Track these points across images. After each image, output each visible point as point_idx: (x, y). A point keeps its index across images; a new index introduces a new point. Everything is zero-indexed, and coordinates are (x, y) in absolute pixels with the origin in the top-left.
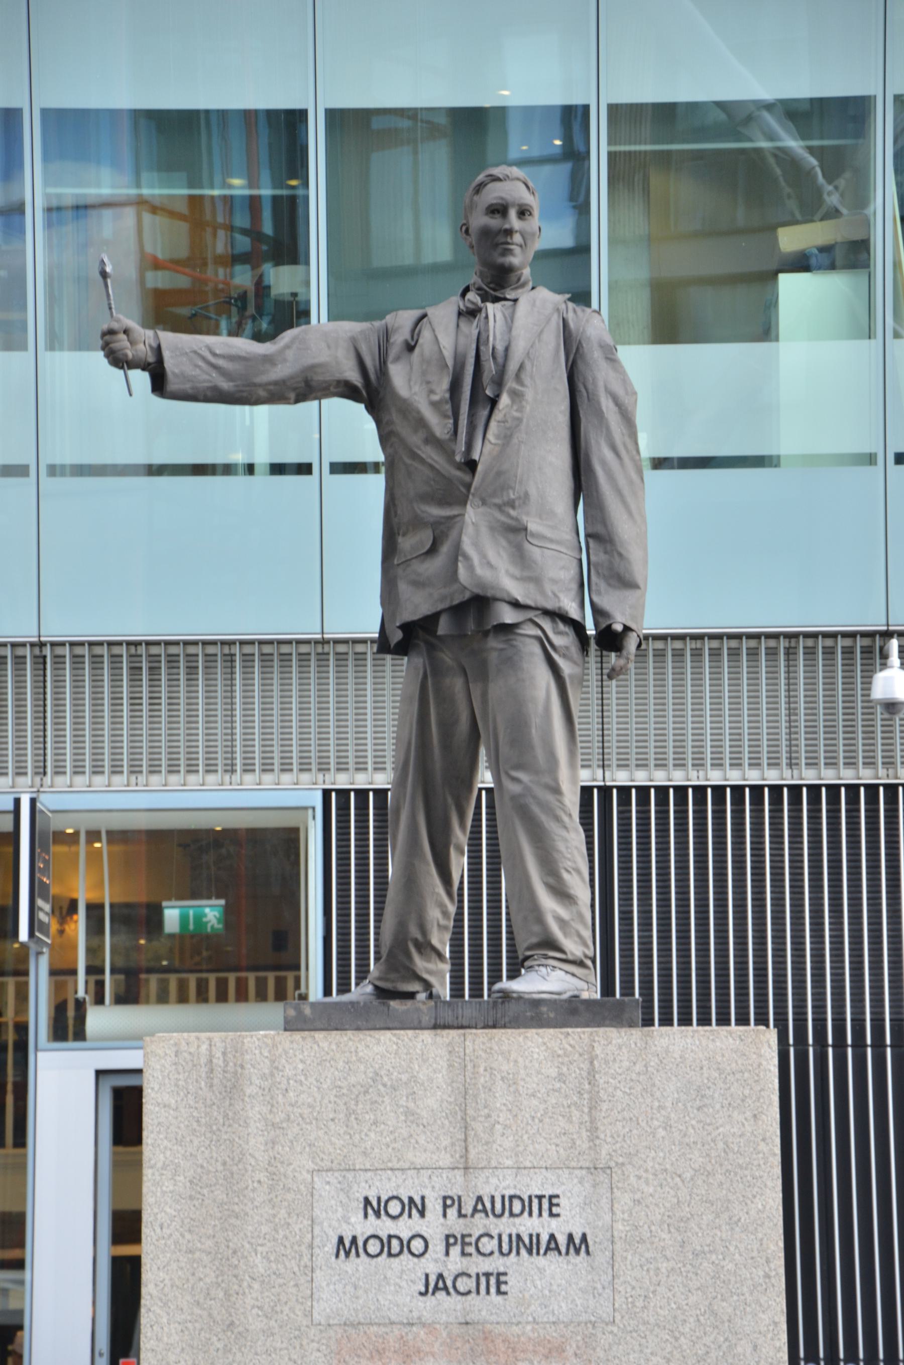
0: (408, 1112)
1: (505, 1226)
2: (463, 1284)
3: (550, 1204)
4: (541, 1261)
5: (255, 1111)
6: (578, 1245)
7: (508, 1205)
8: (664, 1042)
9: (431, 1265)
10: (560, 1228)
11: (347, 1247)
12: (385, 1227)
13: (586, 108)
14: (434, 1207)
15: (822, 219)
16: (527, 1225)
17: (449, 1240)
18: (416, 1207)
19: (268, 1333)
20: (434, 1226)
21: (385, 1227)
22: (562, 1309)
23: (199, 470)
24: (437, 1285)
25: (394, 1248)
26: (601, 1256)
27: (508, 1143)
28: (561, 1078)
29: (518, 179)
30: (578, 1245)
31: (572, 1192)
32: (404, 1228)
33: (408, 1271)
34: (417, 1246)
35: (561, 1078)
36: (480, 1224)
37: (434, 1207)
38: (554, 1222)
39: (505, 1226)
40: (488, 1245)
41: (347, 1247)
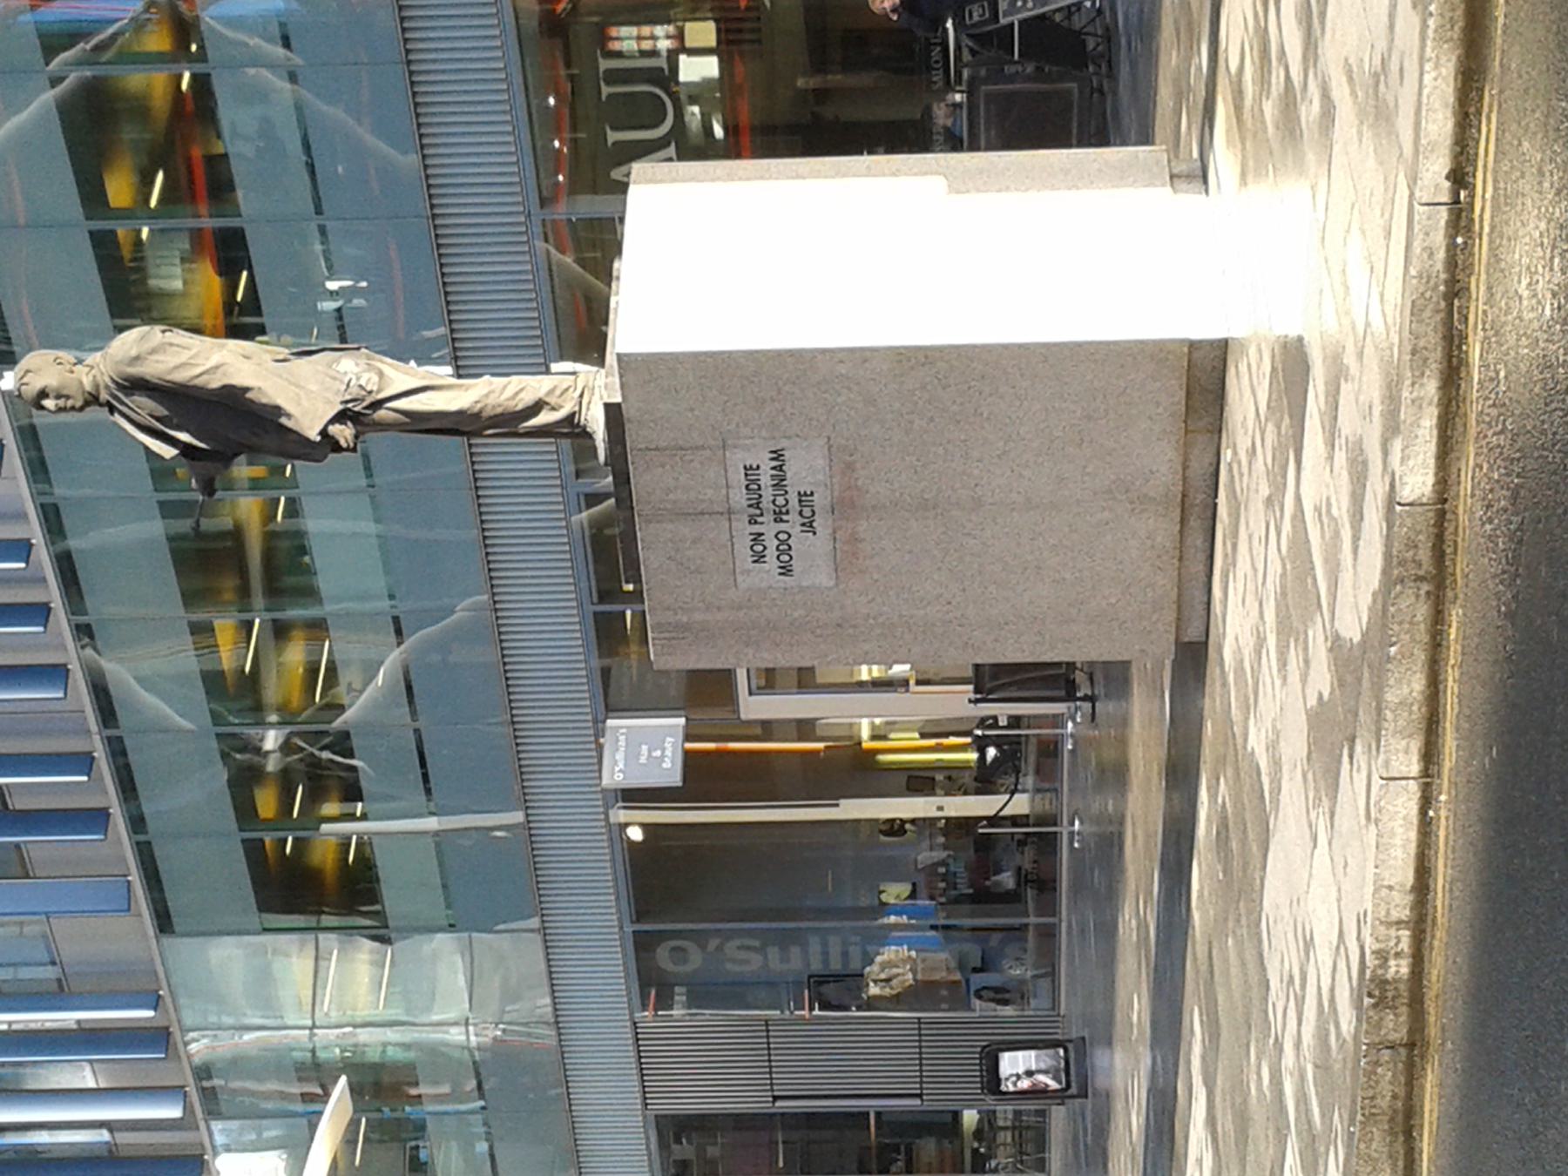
0: (694, 542)
1: (768, 494)
4: (789, 475)
5: (698, 616)
6: (777, 455)
7: (752, 486)
8: (632, 412)
9: (796, 530)
10: (767, 466)
11: (786, 570)
12: (771, 553)
13: (751, 694)
14: (756, 528)
15: (211, 711)
16: (766, 480)
17: (778, 520)
19: (842, 608)
20: (769, 528)
21: (771, 553)
22: (821, 462)
23: (423, 764)
24: (809, 526)
25: (785, 548)
26: (784, 443)
27: (710, 492)
28: (663, 466)
29: (1400, 148)
30: (777, 455)
31: (739, 459)
32: (772, 544)
34: (783, 537)
35: (663, 466)
36: (766, 503)
37: (756, 528)
38: (763, 467)
40: (780, 501)
41: (786, 570)
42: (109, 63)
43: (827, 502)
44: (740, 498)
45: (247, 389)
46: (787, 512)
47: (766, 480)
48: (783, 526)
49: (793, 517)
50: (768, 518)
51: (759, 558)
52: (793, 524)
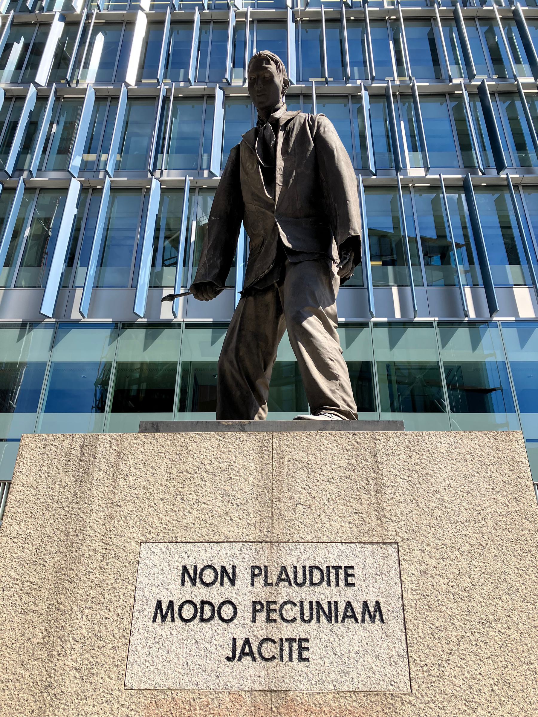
0: (225, 494)
1: (306, 594)
2: (269, 650)
3: (346, 574)
4: (339, 628)
7: (311, 575)
11: (164, 612)
12: (199, 594)
14: (243, 576)
16: (326, 594)
17: (256, 607)
18: (227, 575)
20: (243, 593)
21: (199, 594)
24: (242, 651)
25: (205, 613)
26: (394, 625)
30: (374, 613)
31: (366, 561)
32: (216, 595)
33: (217, 637)
36: (285, 592)
37: (243, 576)
38: (350, 591)
39: (306, 594)
41: (164, 612)
42: (155, 280)
43: (287, 684)
44: (295, 557)
45: (349, 201)
46: (269, 620)
47: (326, 594)
48: (245, 612)
49: (260, 629)
50: (261, 592)
51: (190, 576)
52: (243, 628)
